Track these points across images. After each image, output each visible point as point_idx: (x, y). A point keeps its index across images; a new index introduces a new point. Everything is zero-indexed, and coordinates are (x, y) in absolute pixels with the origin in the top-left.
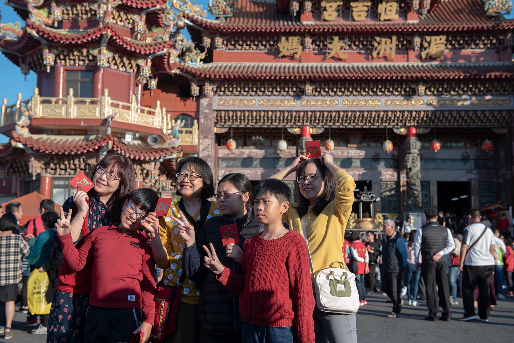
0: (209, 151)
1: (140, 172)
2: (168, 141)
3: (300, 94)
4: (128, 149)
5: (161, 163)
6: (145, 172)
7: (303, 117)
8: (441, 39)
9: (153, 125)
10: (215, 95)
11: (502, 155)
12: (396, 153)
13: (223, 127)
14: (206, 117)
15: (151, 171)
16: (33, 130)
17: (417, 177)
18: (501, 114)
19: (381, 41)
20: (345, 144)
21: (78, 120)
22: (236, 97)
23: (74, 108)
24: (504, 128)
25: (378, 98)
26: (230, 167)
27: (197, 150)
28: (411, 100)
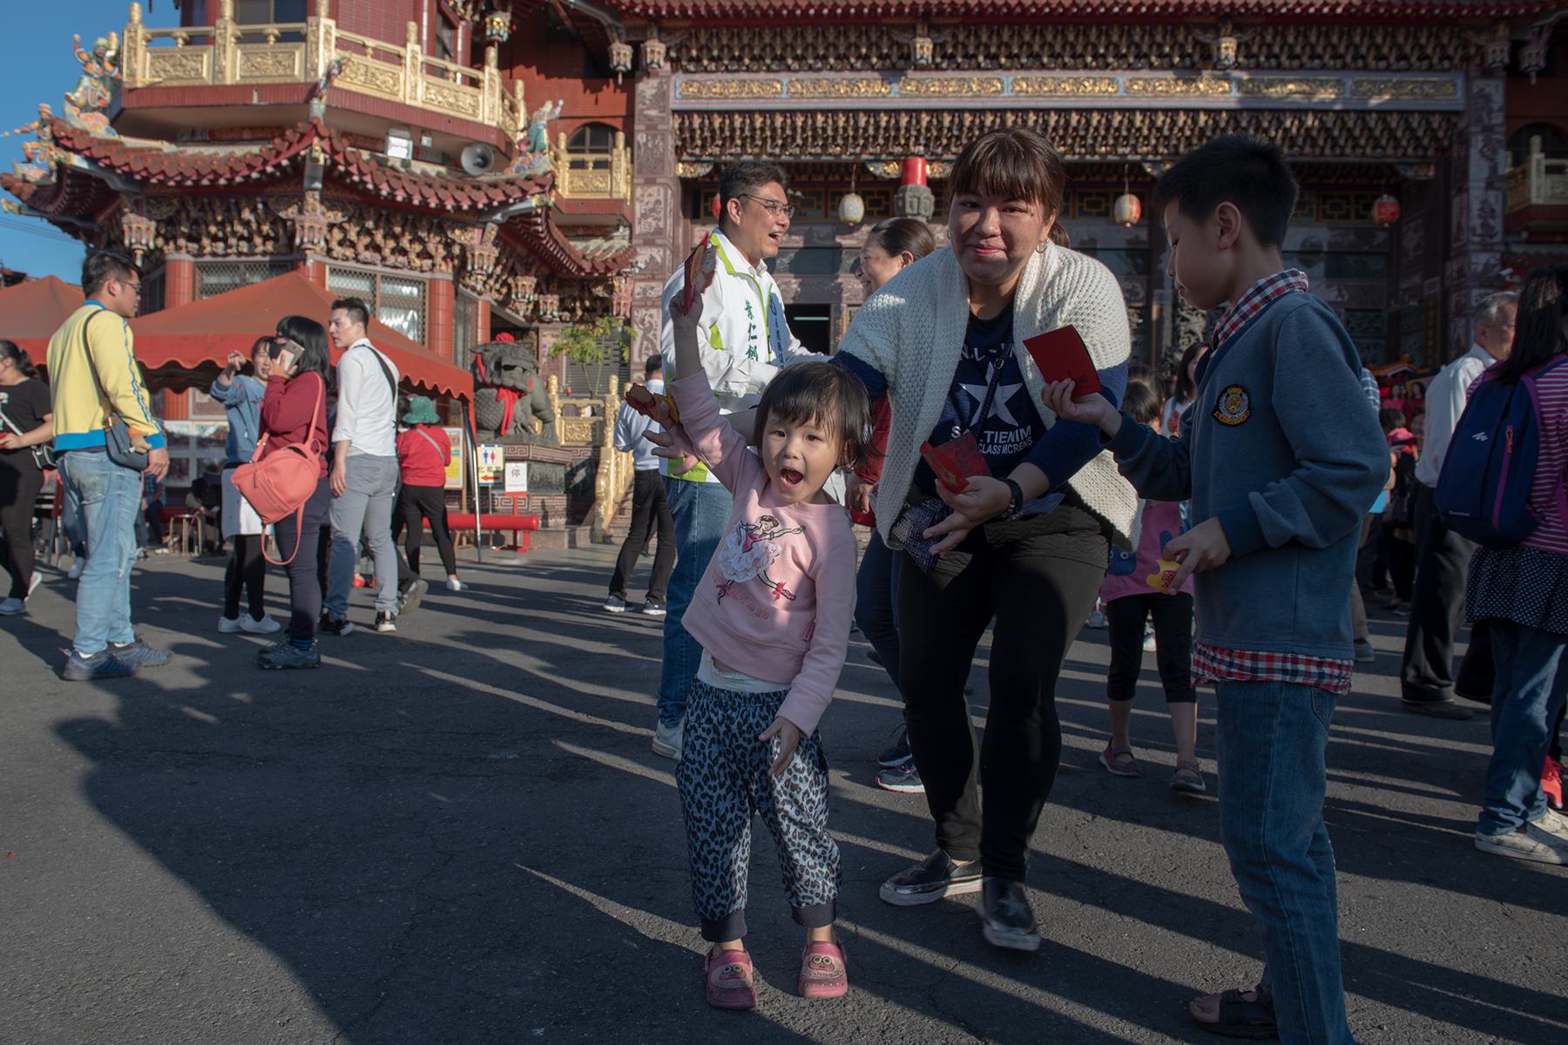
1: (442, 251)
2: (517, 161)
3: (898, 64)
5: (500, 225)
6: (456, 250)
7: (907, 130)
9: (475, 114)
10: (674, 70)
12: (1143, 235)
13: (698, 161)
14: (651, 128)
16: (121, 121)
18: (1429, 123)
21: (243, 89)
22: (729, 76)
23: (234, 55)
25: (1108, 73)
28: (1194, 81)
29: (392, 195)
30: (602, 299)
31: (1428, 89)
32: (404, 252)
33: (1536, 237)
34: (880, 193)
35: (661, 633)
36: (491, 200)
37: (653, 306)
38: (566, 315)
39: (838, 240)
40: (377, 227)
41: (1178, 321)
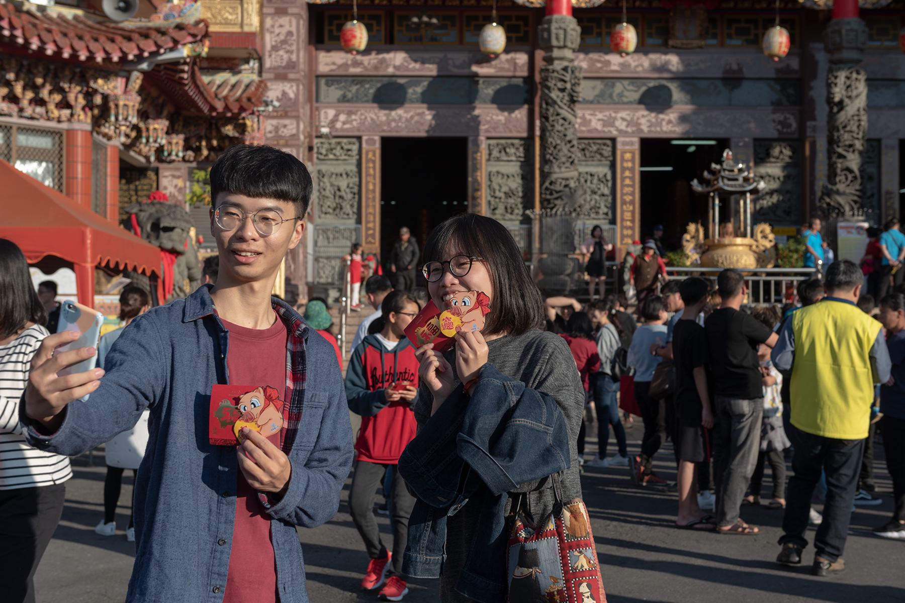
0: (291, 52)
1: (82, 101)
4: (35, 26)
5: (144, 72)
6: (98, 100)
12: (795, 64)
15: (116, 98)
17: (859, 126)
20: (659, 41)
26: (348, 101)
27: (258, 48)
29: (41, 49)
30: (232, 139)
32: (41, 102)
34: (518, 18)
35: (102, 509)
36: (141, 51)
38: (190, 154)
39: (475, 68)
40: (17, 79)
41: (834, 159)
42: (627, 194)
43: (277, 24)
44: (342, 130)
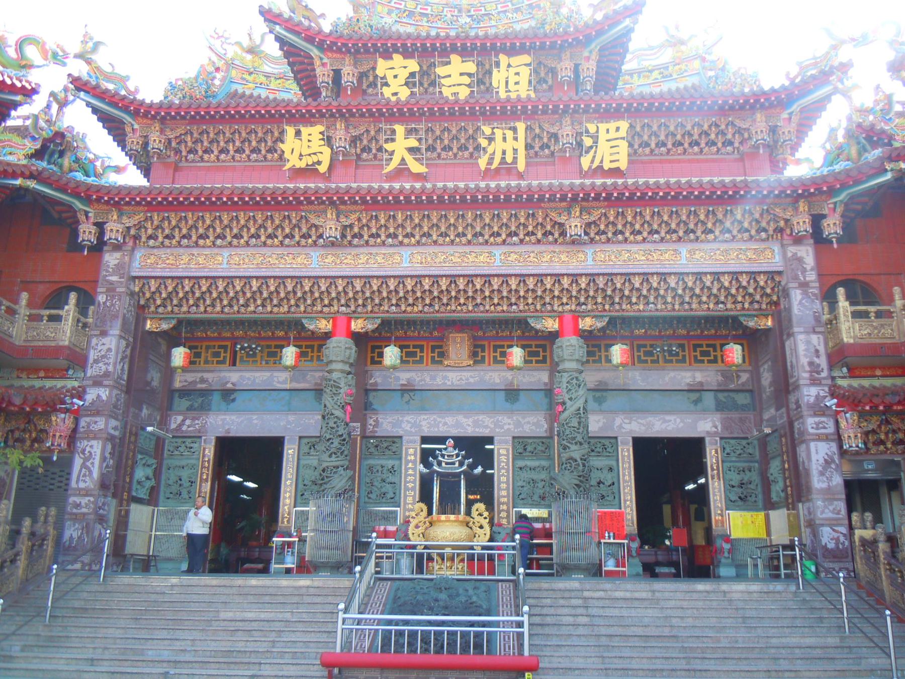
8: (618, 129)
11: (766, 378)
19: (493, 133)
24: (766, 316)
26: (195, 410)
31: (750, 254)
33: (853, 373)
37: (95, 438)
42: (409, 482)
43: (101, 343)
44: (186, 431)
